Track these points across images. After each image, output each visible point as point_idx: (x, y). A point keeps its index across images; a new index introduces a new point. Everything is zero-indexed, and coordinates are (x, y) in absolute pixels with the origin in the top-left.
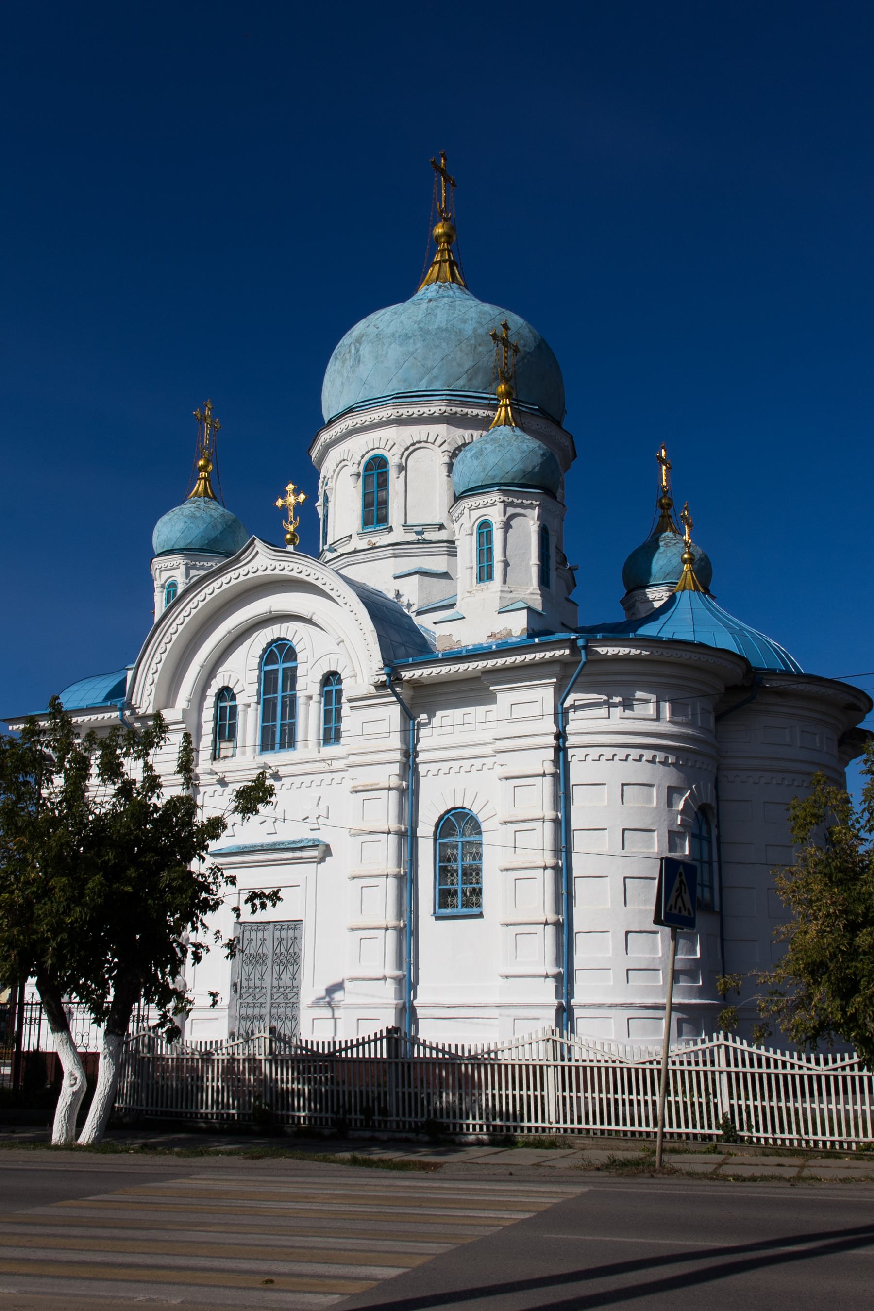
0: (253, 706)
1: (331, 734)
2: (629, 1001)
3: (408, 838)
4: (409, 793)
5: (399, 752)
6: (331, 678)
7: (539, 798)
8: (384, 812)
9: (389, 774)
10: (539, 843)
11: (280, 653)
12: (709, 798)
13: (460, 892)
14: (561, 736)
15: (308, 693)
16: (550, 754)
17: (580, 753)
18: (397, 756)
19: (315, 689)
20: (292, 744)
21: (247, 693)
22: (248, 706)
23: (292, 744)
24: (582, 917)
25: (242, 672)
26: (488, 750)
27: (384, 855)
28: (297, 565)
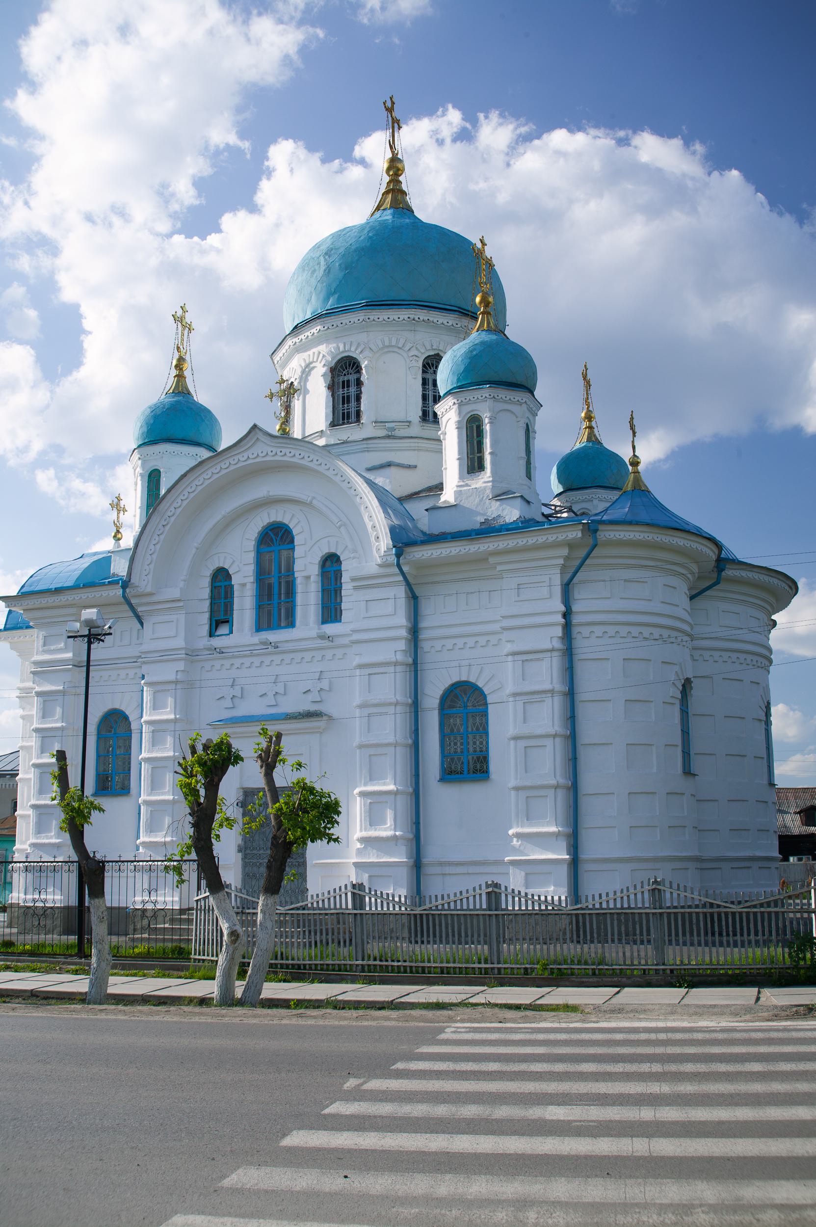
0: (249, 586)
1: (331, 611)
2: (639, 854)
3: (415, 707)
4: (415, 667)
5: (404, 641)
6: (331, 564)
7: (547, 674)
8: (391, 688)
9: (396, 650)
10: (548, 718)
11: (277, 537)
12: (447, 801)
13: (468, 763)
14: (567, 615)
15: (305, 574)
16: (559, 631)
17: (586, 631)
18: (404, 633)
19: (314, 570)
20: (291, 624)
21: (244, 578)
22: (244, 585)
23: (291, 624)
24: (589, 782)
25: (241, 560)
26: (496, 627)
27: (391, 729)
28: (288, 450)
